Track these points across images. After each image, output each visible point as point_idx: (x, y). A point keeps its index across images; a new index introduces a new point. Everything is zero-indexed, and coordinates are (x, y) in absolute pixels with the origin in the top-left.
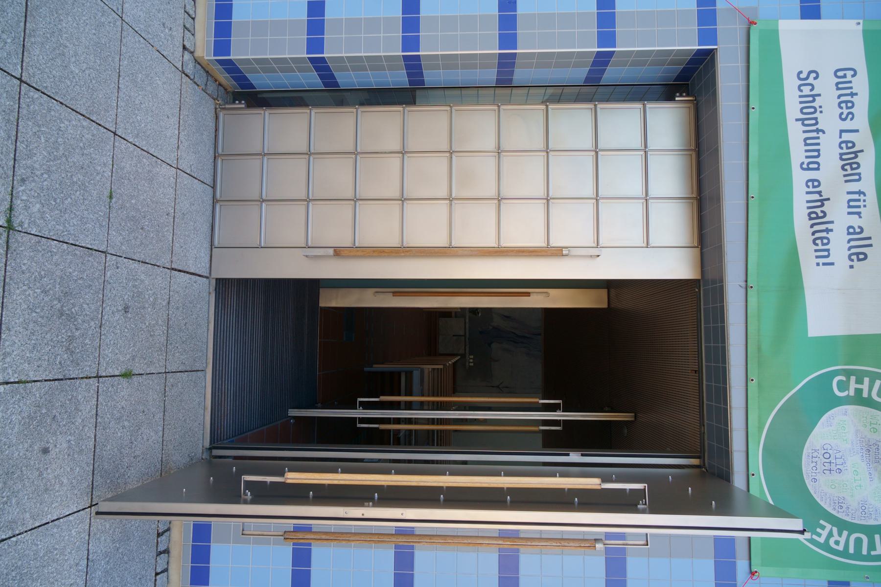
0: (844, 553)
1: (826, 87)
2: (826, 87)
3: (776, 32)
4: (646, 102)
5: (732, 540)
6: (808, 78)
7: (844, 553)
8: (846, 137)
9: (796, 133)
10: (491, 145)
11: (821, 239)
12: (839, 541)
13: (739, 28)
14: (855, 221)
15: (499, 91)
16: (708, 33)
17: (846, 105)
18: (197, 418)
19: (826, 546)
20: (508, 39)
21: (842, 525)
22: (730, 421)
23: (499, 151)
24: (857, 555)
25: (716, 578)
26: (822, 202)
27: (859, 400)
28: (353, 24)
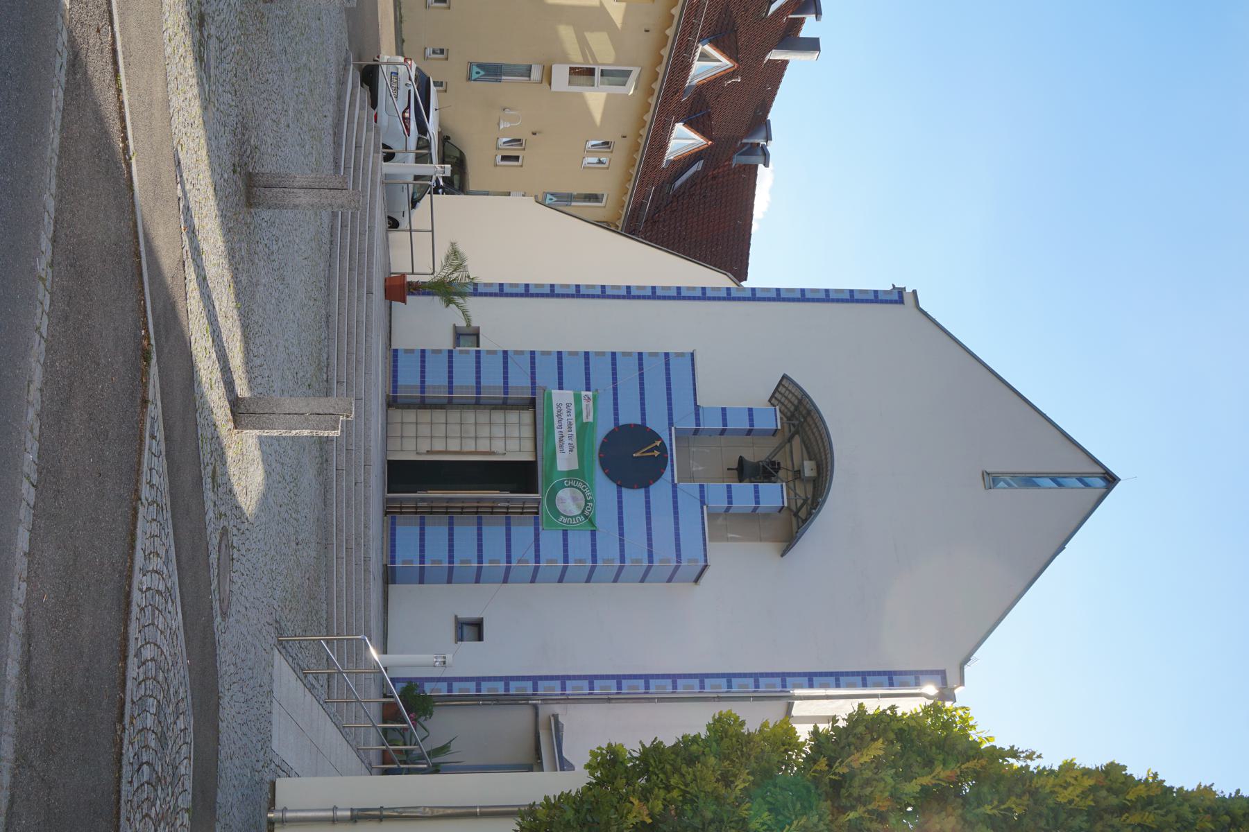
0: (579, 481)
1: (564, 407)
2: (564, 407)
4: (630, 89)
5: (625, 232)
6: (559, 405)
8: (569, 420)
9: (556, 419)
11: (561, 446)
12: (565, 520)
14: (570, 442)
15: (477, 406)
16: (534, 393)
17: (569, 412)
18: (253, 816)
19: (561, 522)
20: (478, 392)
21: (566, 517)
23: (476, 423)
24: (569, 524)
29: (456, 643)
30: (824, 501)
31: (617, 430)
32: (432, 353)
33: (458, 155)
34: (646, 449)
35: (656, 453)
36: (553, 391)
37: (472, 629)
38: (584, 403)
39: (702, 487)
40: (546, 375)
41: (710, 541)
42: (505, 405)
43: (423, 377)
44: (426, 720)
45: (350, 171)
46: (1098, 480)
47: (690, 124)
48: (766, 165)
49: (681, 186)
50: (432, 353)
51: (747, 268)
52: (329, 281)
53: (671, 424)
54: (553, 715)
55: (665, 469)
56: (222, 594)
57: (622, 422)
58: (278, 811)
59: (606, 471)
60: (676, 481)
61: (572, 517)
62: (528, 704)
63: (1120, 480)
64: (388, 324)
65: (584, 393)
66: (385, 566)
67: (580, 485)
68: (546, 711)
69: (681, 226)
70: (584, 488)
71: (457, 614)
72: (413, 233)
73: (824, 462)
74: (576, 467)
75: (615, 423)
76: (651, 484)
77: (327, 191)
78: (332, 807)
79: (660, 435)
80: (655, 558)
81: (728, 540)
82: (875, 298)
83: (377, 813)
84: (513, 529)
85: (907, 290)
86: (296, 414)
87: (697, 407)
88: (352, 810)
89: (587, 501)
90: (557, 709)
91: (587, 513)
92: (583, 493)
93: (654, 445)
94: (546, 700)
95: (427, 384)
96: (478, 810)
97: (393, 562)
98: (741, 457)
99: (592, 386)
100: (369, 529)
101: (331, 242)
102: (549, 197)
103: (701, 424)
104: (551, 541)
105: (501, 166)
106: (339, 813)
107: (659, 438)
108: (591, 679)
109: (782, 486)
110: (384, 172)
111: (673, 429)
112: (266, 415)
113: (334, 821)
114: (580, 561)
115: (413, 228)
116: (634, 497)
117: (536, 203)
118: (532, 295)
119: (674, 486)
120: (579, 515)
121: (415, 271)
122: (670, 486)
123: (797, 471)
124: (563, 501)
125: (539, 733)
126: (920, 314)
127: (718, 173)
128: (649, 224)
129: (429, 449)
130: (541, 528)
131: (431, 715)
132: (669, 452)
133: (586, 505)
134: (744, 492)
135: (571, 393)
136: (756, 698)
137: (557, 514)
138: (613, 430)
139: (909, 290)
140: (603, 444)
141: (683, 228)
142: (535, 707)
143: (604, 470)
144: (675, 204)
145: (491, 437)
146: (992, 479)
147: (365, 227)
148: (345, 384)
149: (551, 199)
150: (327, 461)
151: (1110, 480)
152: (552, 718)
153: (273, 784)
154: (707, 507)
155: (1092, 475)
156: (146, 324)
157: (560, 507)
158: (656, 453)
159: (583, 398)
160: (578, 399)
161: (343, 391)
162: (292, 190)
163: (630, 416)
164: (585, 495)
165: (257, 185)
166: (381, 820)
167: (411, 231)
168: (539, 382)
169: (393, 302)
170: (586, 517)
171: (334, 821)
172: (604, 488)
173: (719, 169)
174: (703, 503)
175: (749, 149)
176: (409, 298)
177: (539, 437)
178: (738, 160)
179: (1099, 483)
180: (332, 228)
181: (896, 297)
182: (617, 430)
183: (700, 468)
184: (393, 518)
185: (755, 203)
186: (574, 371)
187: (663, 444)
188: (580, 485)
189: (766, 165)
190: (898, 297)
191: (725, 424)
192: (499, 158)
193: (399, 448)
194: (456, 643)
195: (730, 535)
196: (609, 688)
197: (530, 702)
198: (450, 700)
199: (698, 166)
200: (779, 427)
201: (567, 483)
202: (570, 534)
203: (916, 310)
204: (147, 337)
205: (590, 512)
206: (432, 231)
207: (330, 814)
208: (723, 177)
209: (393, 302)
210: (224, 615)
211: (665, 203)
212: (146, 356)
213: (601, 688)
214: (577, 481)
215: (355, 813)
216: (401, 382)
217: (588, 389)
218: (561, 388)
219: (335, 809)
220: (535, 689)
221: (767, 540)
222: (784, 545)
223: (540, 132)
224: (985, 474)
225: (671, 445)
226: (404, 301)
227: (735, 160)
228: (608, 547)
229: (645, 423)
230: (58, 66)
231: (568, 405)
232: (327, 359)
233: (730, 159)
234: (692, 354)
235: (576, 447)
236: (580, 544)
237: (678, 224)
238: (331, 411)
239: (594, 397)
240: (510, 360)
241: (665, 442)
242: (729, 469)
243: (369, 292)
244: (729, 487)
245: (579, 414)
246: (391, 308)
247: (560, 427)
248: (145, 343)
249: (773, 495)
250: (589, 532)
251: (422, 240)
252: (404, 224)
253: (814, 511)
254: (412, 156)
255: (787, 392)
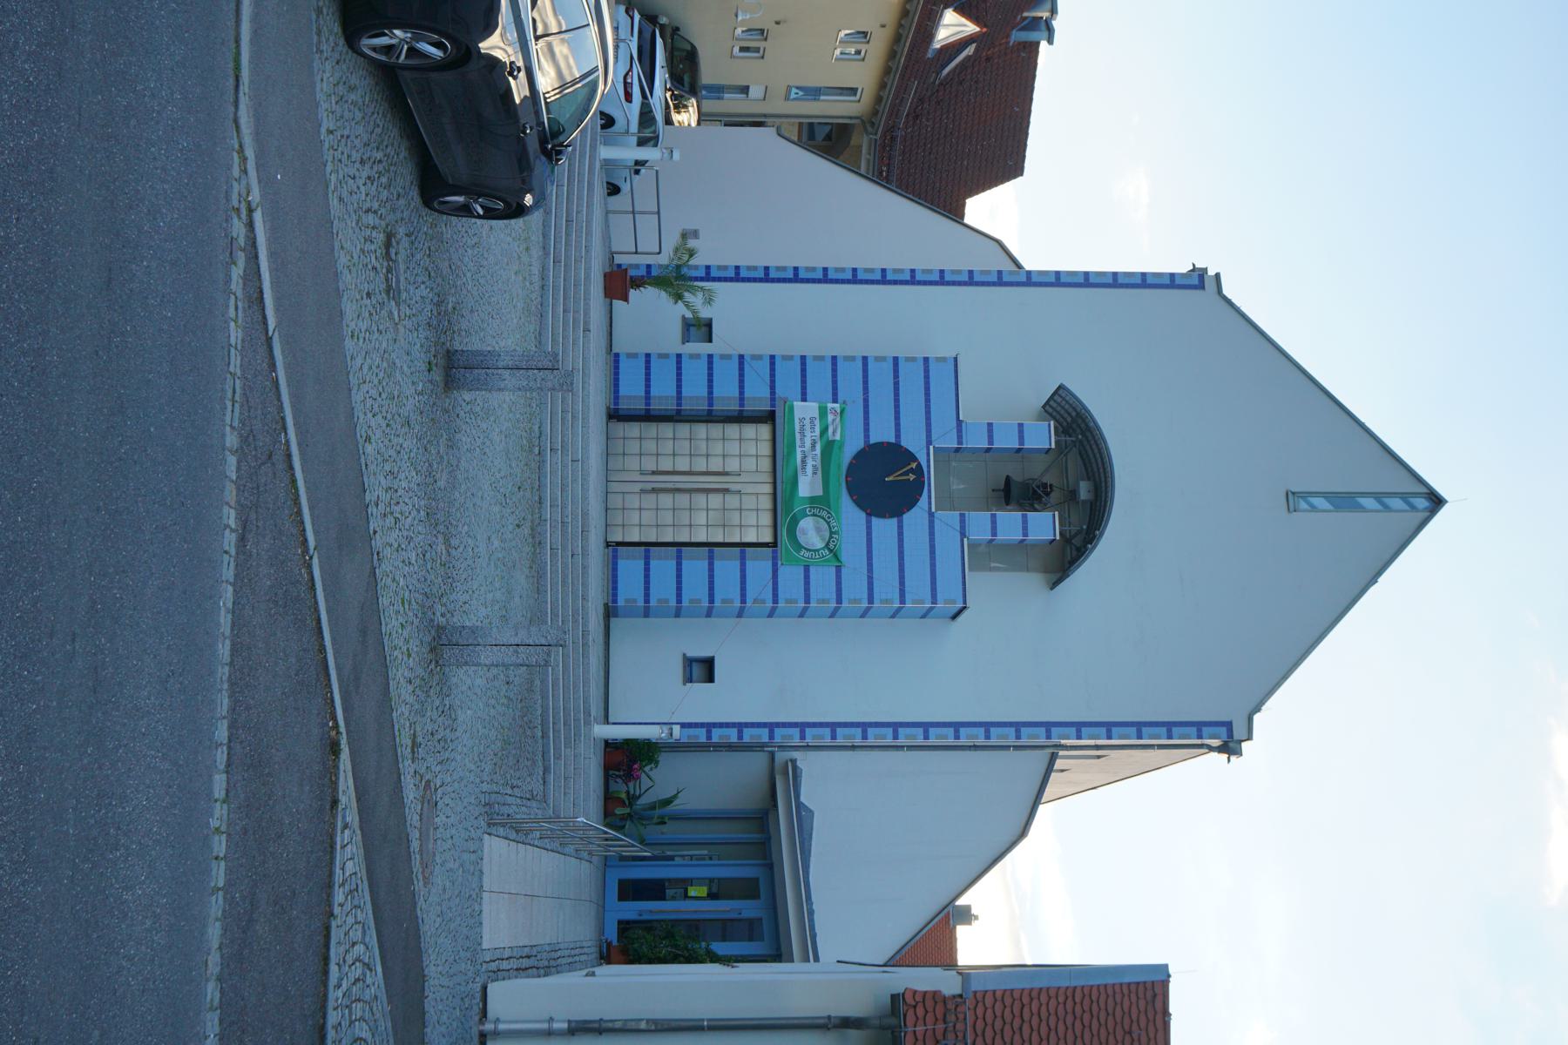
0: (824, 510)
1: (807, 422)
2: (807, 422)
3: (793, 405)
6: (802, 420)
7: (824, 510)
9: (798, 436)
10: (705, 437)
11: (804, 468)
12: (807, 554)
13: (782, 403)
16: (773, 405)
17: (813, 428)
19: (803, 556)
22: (517, 1022)
23: (707, 439)
25: (629, 901)
26: (805, 457)
27: (814, 515)
28: (629, 397)
29: (684, 684)
30: (1102, 534)
31: (867, 449)
32: (659, 358)
33: (689, 48)
34: (899, 473)
35: (912, 477)
36: (795, 403)
37: (702, 669)
38: (830, 417)
39: (962, 516)
40: (788, 384)
41: (970, 570)
42: (741, 418)
43: (648, 386)
44: (651, 769)
45: (563, 190)
46: (1423, 500)
47: (961, 10)
48: (1050, 41)
49: (948, 74)
50: (659, 358)
51: (1025, 151)
52: (540, 334)
53: (929, 442)
54: (791, 760)
55: (920, 496)
56: (424, 856)
57: (872, 441)
58: (490, 1022)
59: (854, 498)
60: (933, 510)
61: (815, 551)
62: (764, 751)
63: (1446, 502)
64: (609, 316)
65: (830, 405)
66: (606, 605)
67: (824, 514)
68: (781, 757)
69: (947, 118)
70: (829, 518)
71: (685, 652)
72: (637, 216)
73: (1103, 484)
74: (820, 492)
75: (865, 442)
76: (904, 513)
77: (536, 371)
78: (548, 1018)
79: (917, 456)
80: (908, 597)
81: (991, 569)
82: (1171, 282)
83: (596, 1025)
84: (749, 563)
85: (1209, 273)
86: (503, 645)
87: (959, 423)
88: (569, 1022)
89: (831, 533)
90: (795, 755)
91: (831, 546)
92: (828, 523)
93: (909, 467)
94: (782, 748)
95: (652, 394)
96: (705, 1023)
97: (615, 601)
98: (1008, 476)
99: (841, 397)
100: (588, 601)
101: (543, 287)
102: (794, 90)
103: (964, 441)
104: (790, 577)
105: (738, 57)
106: (556, 1026)
107: (914, 459)
108: (833, 726)
109: (1054, 515)
110: (601, 158)
111: (931, 447)
112: (470, 647)
113: (549, 1033)
114: (824, 601)
115: (636, 209)
116: (884, 527)
117: (779, 137)
118: (773, 280)
119: (931, 515)
120: (823, 549)
121: (639, 250)
122: (926, 515)
123: (1071, 491)
124: (804, 533)
125: (775, 778)
126: (1223, 302)
127: (993, 53)
128: (911, 118)
129: (655, 469)
130: (779, 563)
131: (657, 763)
132: (926, 477)
133: (831, 537)
134: (1010, 523)
135: (815, 405)
136: (1017, 748)
137: (799, 547)
138: (862, 450)
139: (1211, 272)
140: (851, 466)
141: (951, 120)
142: (772, 755)
143: (852, 497)
144: (941, 93)
145: (724, 509)
146: (1293, 499)
147: (581, 253)
148: (560, 452)
149: (797, 93)
150: (540, 543)
151: (1436, 501)
152: (790, 764)
153: (485, 989)
154: (968, 539)
155: (1416, 495)
156: (334, 718)
157: (802, 539)
158: (912, 477)
159: (829, 411)
160: (823, 412)
161: (558, 459)
162: (495, 372)
163: (882, 433)
164: (829, 526)
165: (456, 365)
166: (600, 1034)
167: (633, 212)
168: (779, 392)
169: (614, 301)
170: (831, 551)
171: (549, 1033)
172: (850, 515)
173: (994, 48)
174: (963, 535)
175: (1028, 24)
176: (632, 293)
177: (779, 482)
178: (1017, 36)
179: (1422, 503)
180: (544, 268)
181: (1196, 282)
182: (867, 449)
183: (962, 486)
184: (615, 551)
185: (1035, 96)
186: (819, 379)
187: (919, 465)
188: (824, 514)
189: (1050, 41)
190: (1198, 280)
191: (991, 441)
192: (736, 49)
193: (622, 468)
194: (684, 684)
195: (993, 565)
196: (853, 737)
197: (766, 749)
198: (676, 747)
199: (970, 50)
200: (1053, 446)
201: (810, 511)
202: (812, 570)
203: (1217, 297)
204: (336, 726)
205: (835, 546)
206: (658, 213)
207: (545, 1026)
208: (999, 57)
209: (614, 301)
210: (426, 882)
211: (929, 93)
212: (335, 748)
213: (845, 737)
214: (820, 509)
215: (573, 1025)
216: (623, 391)
217: (835, 401)
218: (804, 399)
219: (551, 1020)
220: (771, 736)
221: (1035, 570)
222: (1055, 577)
223: (785, 22)
224: (1289, 493)
225: (929, 466)
226: (626, 299)
227: (1013, 37)
228: (855, 586)
229: (900, 442)
230: (226, 563)
231: (812, 420)
232: (539, 428)
233: (1008, 36)
234: (956, 359)
235: (820, 469)
236: (823, 579)
237: (945, 116)
238: (544, 642)
239: (842, 412)
240: (746, 367)
241: (922, 463)
242: (993, 490)
243: (586, 330)
244: (993, 516)
245: (824, 431)
246: (611, 304)
247: (803, 446)
248: (333, 733)
249: (1044, 525)
250: (834, 569)
251: (647, 225)
252: (625, 188)
253: (1089, 546)
254: (634, 140)
255: (1064, 402)
